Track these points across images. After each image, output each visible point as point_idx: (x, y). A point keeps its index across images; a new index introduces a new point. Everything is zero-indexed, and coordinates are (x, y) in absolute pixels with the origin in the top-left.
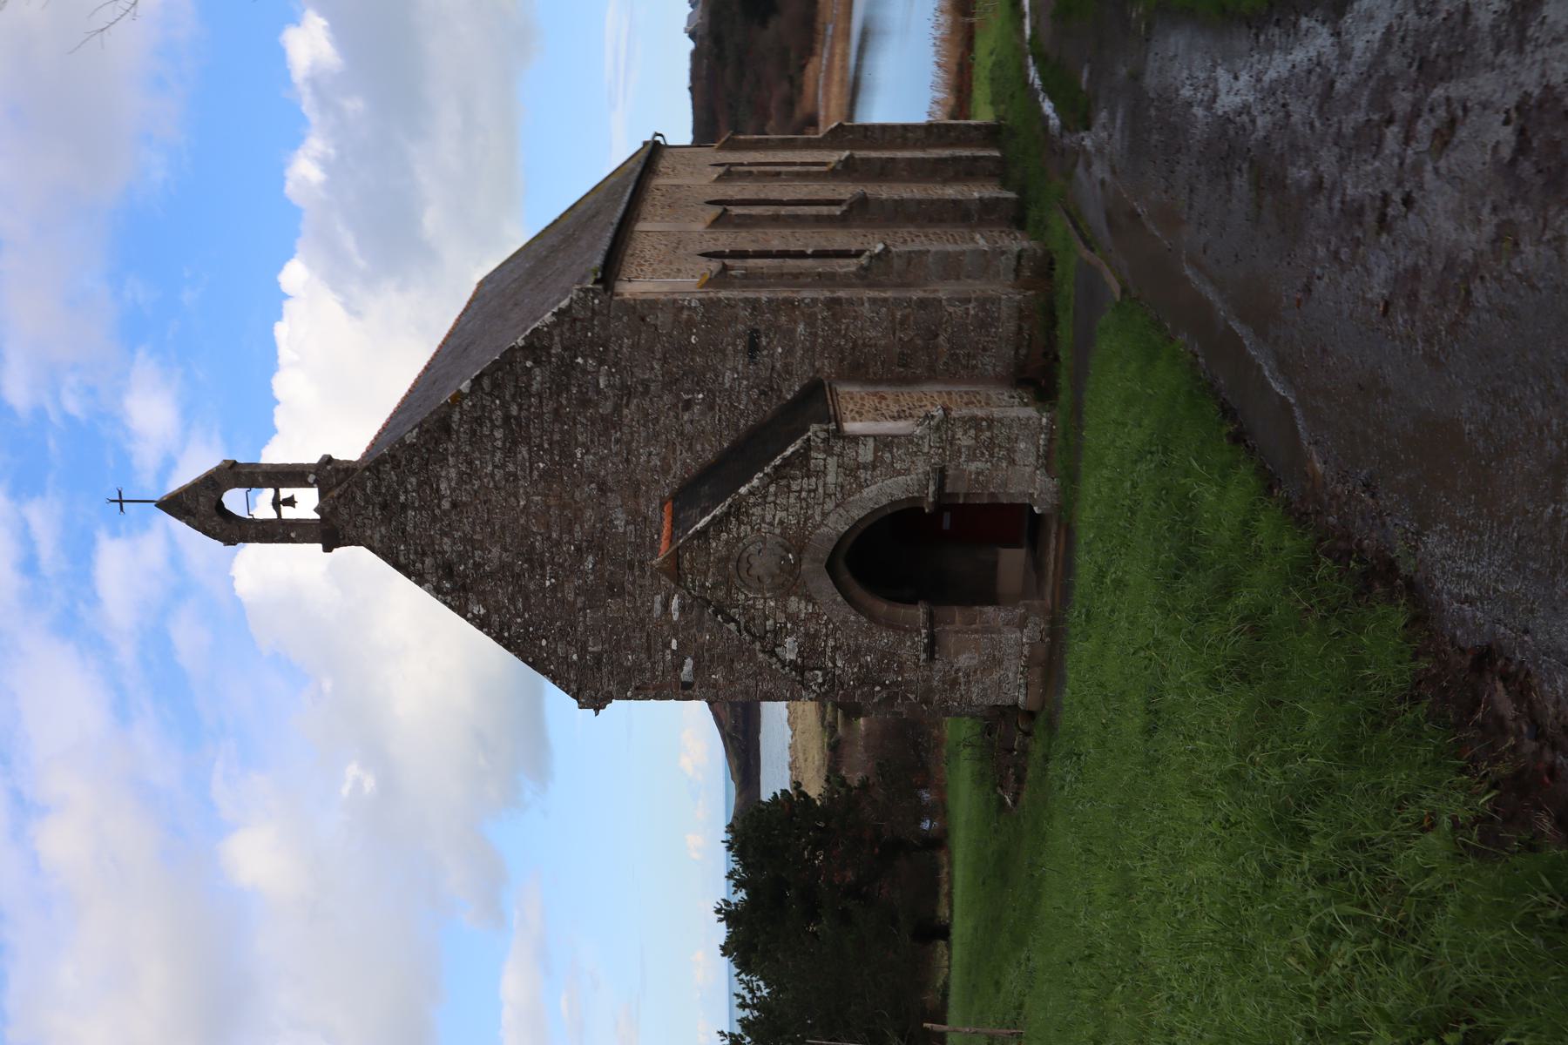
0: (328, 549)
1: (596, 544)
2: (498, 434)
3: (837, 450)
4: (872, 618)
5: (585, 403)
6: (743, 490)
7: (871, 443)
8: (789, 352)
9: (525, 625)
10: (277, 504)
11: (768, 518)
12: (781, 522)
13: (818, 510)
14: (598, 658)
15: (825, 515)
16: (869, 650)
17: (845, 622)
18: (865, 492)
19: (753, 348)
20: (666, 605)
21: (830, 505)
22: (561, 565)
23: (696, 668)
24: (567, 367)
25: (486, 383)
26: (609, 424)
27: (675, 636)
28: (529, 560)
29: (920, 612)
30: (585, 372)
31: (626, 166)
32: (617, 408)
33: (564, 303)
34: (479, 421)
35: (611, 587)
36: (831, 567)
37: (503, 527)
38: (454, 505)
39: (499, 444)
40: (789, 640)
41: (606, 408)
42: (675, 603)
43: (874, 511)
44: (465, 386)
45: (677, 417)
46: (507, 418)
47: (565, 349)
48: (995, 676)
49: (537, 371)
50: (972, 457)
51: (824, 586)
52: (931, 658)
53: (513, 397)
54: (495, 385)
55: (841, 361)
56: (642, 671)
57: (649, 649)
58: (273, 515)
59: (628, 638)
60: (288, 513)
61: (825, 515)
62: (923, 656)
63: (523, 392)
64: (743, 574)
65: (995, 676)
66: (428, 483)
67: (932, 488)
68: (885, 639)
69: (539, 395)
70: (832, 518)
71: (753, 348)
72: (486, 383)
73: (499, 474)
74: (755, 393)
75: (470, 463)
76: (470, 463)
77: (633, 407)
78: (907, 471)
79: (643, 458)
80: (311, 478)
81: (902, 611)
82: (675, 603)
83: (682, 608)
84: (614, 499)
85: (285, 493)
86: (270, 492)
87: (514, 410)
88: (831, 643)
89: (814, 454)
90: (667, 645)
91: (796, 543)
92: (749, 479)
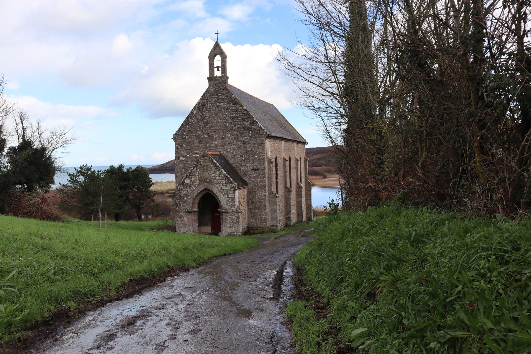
0: (208, 78)
1: (210, 137)
2: (234, 115)
3: (232, 189)
4: (195, 199)
5: (241, 134)
6: (222, 170)
7: (233, 196)
8: (254, 178)
9: (191, 122)
10: (218, 67)
11: (216, 175)
12: (215, 178)
13: (218, 186)
14: (184, 139)
15: (217, 187)
16: (188, 199)
17: (194, 193)
18: (222, 196)
19: (254, 170)
20: (197, 153)
21: (219, 188)
22: (205, 130)
23: (183, 161)
24: (249, 129)
25: (245, 112)
26: (237, 139)
27: (190, 156)
28: (206, 123)
29: (196, 209)
30: (248, 133)
31: (286, 123)
32: (240, 141)
33: (263, 128)
34: (237, 111)
35: (200, 141)
36: (206, 189)
37: (213, 117)
38: (218, 106)
39: (232, 115)
40: (189, 181)
41: (240, 138)
42: (197, 155)
43: (218, 198)
44: (245, 108)
45: (239, 154)
46: (238, 117)
47: (253, 129)
48: (182, 226)
49: (248, 123)
50: (230, 218)
51: (202, 188)
52: (186, 212)
53: (243, 118)
54: (245, 114)
55: (252, 189)
56: (182, 148)
57: (187, 150)
58: (215, 66)
59: (189, 145)
60: (216, 69)
61: (217, 187)
62: (186, 210)
63: (244, 120)
64: (204, 170)
65: (182, 226)
66: (223, 100)
67: (223, 210)
68: (190, 202)
69: (243, 124)
70: (217, 189)
71: (254, 170)
72: (245, 112)
73: (225, 116)
74: (244, 171)
75: (228, 109)
76: (228, 109)
77: (241, 144)
78: (227, 205)
79: (230, 147)
80: (223, 75)
81: (196, 205)
82: (197, 155)
83: (196, 157)
84: (220, 141)
85: (220, 69)
86: (220, 66)
87: (240, 118)
88: (189, 190)
89: (230, 184)
90: (188, 154)
91: (211, 182)
92: (225, 171)
